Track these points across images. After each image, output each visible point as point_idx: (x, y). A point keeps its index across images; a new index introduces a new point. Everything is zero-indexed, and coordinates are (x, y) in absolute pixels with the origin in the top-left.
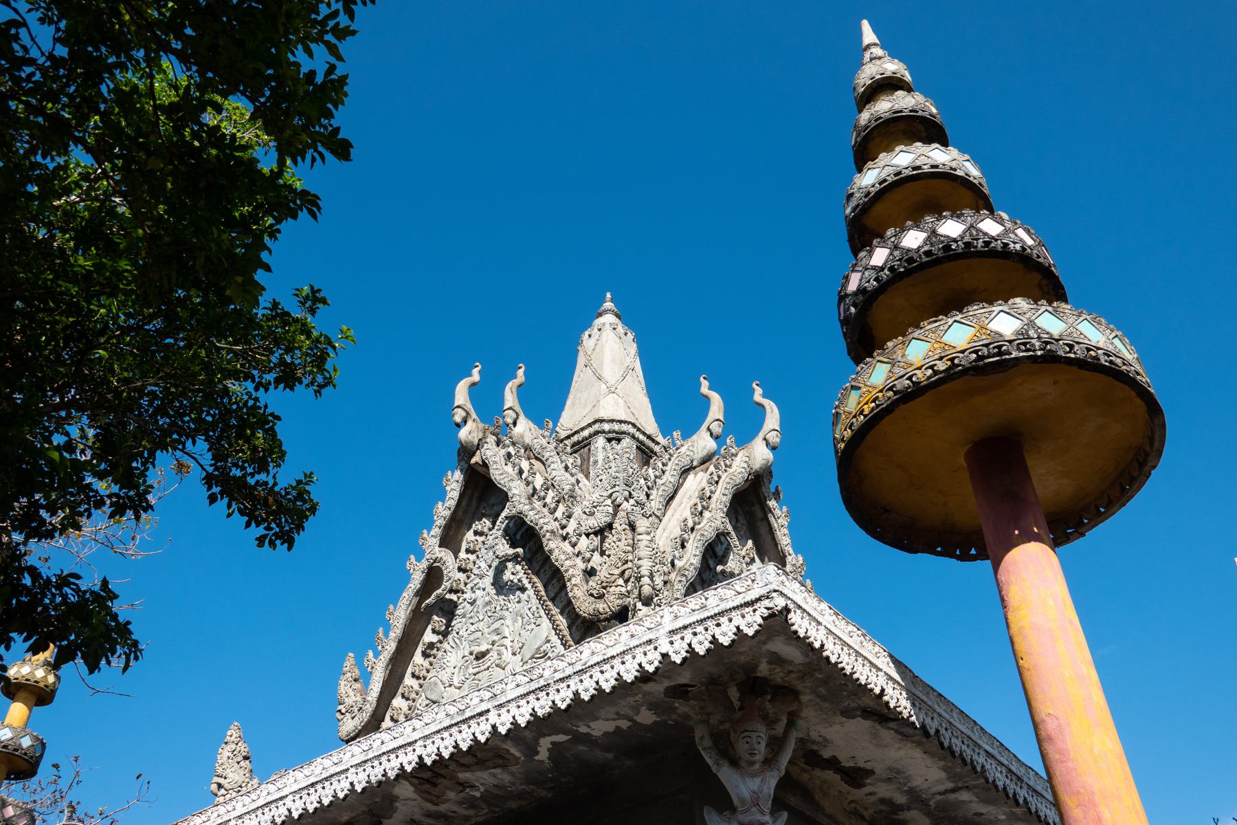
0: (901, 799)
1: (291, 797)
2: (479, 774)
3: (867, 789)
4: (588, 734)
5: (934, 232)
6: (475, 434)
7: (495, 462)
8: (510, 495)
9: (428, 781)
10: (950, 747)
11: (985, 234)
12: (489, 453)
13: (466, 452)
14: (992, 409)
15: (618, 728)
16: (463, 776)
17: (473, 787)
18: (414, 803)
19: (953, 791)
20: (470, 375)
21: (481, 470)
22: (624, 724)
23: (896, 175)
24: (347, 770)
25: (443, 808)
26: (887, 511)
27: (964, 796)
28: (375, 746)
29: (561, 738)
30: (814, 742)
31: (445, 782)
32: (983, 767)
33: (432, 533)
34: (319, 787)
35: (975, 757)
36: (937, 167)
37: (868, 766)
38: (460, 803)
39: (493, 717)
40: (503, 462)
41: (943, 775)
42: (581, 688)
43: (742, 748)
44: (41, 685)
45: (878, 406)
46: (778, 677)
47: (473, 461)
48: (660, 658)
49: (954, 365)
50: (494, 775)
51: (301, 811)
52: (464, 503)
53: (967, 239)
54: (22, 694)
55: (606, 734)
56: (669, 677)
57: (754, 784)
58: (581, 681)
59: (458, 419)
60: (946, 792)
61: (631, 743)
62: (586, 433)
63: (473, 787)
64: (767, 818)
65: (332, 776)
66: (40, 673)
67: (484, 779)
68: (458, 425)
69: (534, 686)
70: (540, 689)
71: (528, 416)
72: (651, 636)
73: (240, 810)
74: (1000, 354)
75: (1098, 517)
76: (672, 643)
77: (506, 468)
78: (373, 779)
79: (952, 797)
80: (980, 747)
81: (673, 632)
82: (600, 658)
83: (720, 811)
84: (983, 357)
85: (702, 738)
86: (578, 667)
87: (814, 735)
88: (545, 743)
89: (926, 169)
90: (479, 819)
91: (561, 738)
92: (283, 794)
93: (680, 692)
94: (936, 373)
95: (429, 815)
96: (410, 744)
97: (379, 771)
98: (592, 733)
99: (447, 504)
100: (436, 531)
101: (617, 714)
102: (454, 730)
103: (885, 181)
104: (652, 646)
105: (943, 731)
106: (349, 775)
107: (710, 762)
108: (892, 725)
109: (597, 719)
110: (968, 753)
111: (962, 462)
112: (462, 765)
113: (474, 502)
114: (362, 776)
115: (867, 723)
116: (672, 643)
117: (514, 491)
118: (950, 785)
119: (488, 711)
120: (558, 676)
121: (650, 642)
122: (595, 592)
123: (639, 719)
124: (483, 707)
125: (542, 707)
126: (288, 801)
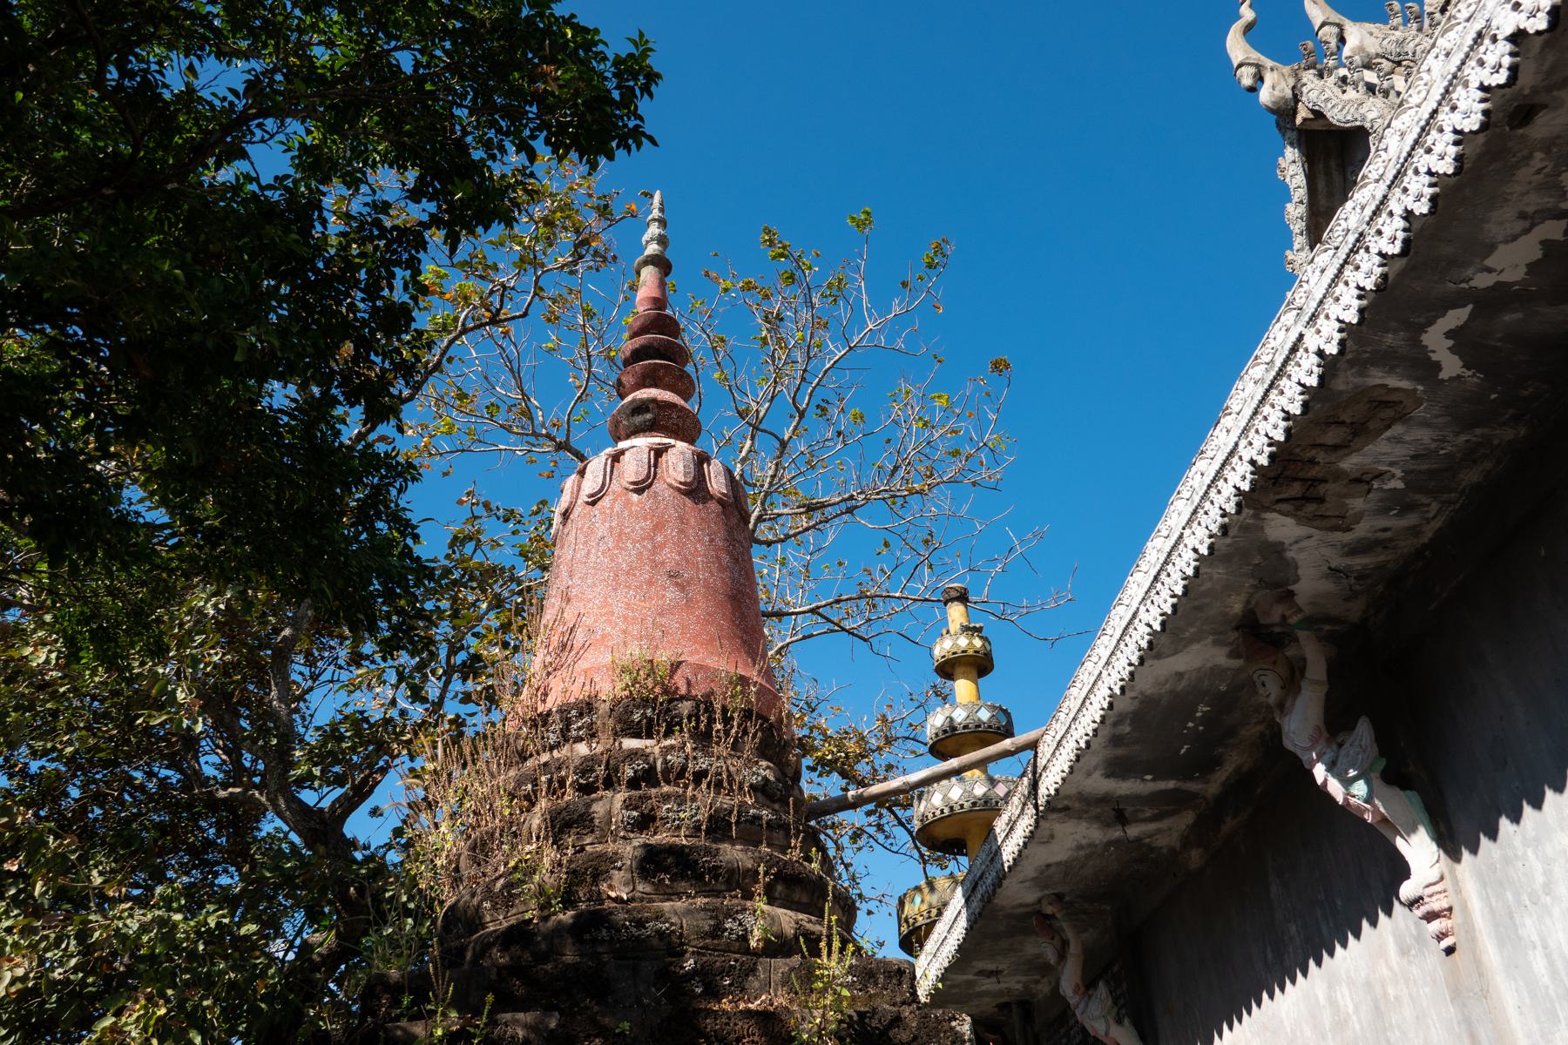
1: (1143, 609)
4: (1498, 284)
6: (1283, 84)
7: (1327, 100)
8: (1368, 125)
9: (1305, 499)
12: (1313, 95)
13: (1284, 112)
15: (1546, 244)
18: (1312, 542)
20: (1239, 17)
21: (1317, 126)
24: (1181, 536)
25: (1362, 530)
28: (1196, 486)
29: (1457, 317)
33: (1296, 246)
34: (1163, 576)
38: (1383, 511)
39: (1312, 342)
40: (1338, 91)
44: (971, 652)
47: (1299, 120)
48: (1508, 47)
51: (1160, 618)
54: (959, 670)
55: (1532, 267)
58: (1405, 190)
59: (1247, 81)
63: (1379, 475)
65: (1169, 554)
66: (963, 642)
67: (1387, 453)
68: (1253, 90)
69: (1342, 255)
71: (1356, 18)
72: (1478, 25)
73: (1105, 654)
77: (1345, 97)
78: (1215, 529)
90: (1437, 524)
91: (1457, 317)
92: (1133, 609)
96: (1232, 453)
97: (1215, 513)
98: (1505, 278)
99: (1296, 199)
100: (1300, 241)
101: (1523, 216)
102: (1273, 395)
104: (1487, 41)
106: (1186, 540)
109: (1491, 248)
113: (1337, 177)
114: (1202, 533)
117: (1370, 116)
119: (1301, 336)
121: (1480, 35)
124: (1293, 336)
125: (1369, 274)
126: (1142, 615)
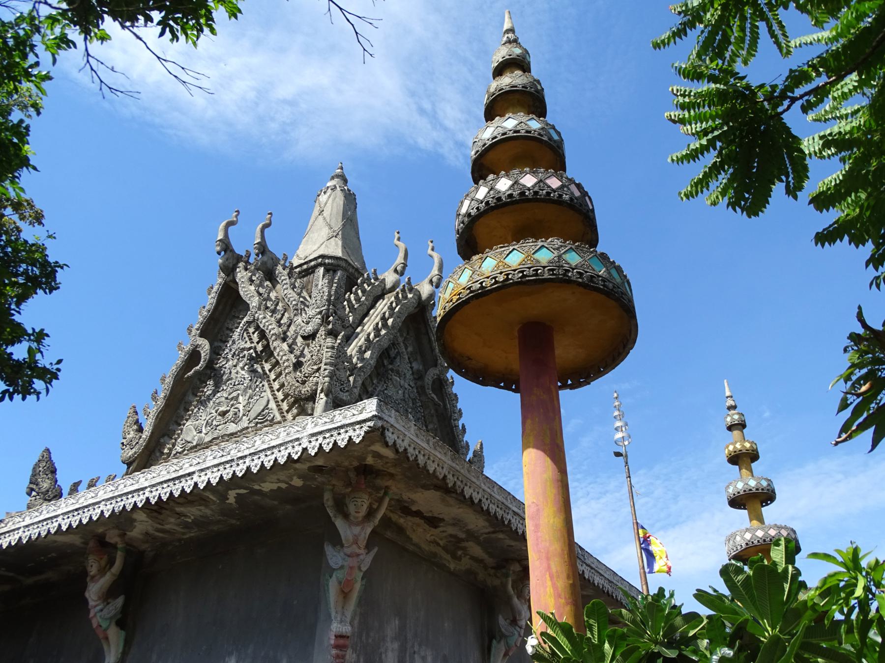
0: (462, 535)
2: (189, 509)
3: (441, 529)
5: (516, 182)
10: (488, 510)
11: (549, 187)
14: (535, 306)
16: (179, 509)
17: (186, 516)
19: (494, 532)
22: (284, 486)
23: (503, 134)
25: (167, 527)
26: (470, 359)
27: (501, 536)
30: (406, 502)
31: (168, 512)
32: (510, 521)
35: (505, 515)
36: (530, 132)
37: (441, 516)
38: (178, 525)
41: (487, 524)
42: (253, 464)
43: (352, 509)
45: (460, 298)
46: (379, 465)
49: (507, 279)
50: (200, 510)
52: (220, 308)
53: (536, 189)
55: (271, 490)
56: (310, 461)
57: (357, 530)
60: (489, 533)
61: (286, 496)
62: (313, 263)
63: (186, 516)
64: (362, 551)
69: (224, 459)
70: (227, 462)
74: (537, 275)
75: (599, 374)
76: (310, 442)
79: (493, 536)
80: (510, 509)
81: (313, 435)
82: (266, 446)
83: (334, 546)
84: (526, 276)
85: (327, 500)
86: (252, 451)
87: (405, 497)
88: (232, 495)
89: (523, 133)
93: (319, 469)
94: (496, 282)
95: (158, 530)
103: (496, 137)
105: (484, 500)
107: (331, 515)
108: (454, 495)
110: (500, 513)
111: (516, 334)
112: (179, 503)
115: (438, 493)
116: (310, 442)
118: (491, 530)
120: (240, 455)
121: (298, 439)
122: (300, 380)
123: (293, 483)
126: (60, 519)
